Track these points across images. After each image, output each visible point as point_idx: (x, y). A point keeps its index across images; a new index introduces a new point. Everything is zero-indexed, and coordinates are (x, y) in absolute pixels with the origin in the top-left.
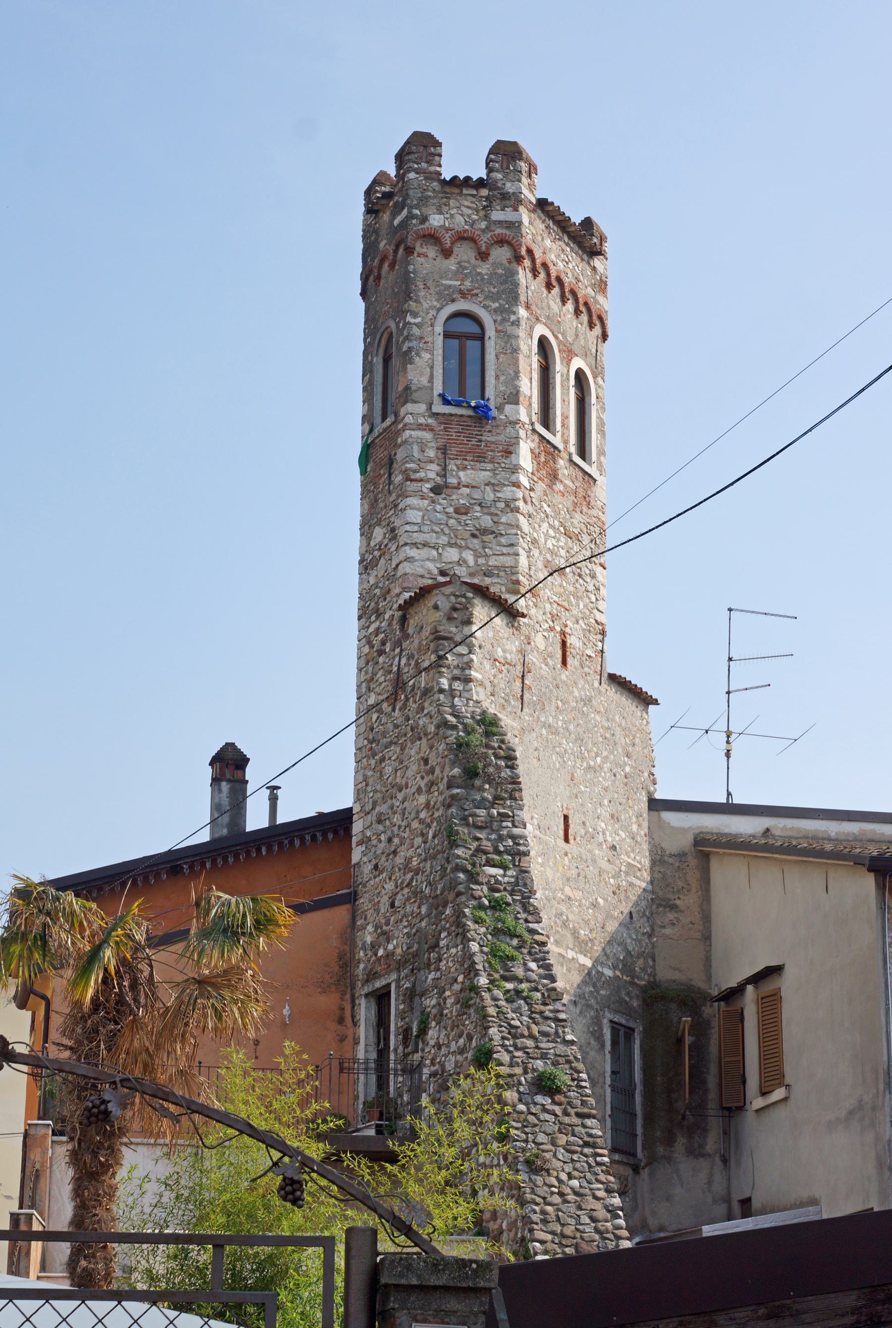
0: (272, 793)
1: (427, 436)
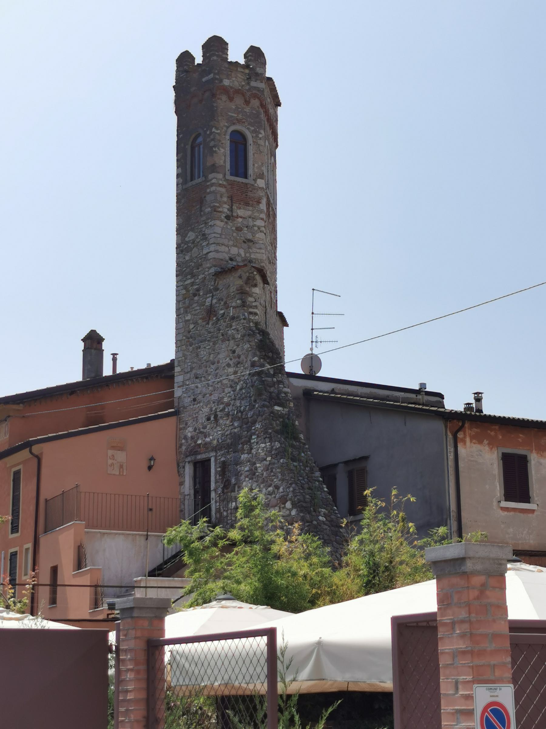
0: (114, 357)
1: (223, 190)
